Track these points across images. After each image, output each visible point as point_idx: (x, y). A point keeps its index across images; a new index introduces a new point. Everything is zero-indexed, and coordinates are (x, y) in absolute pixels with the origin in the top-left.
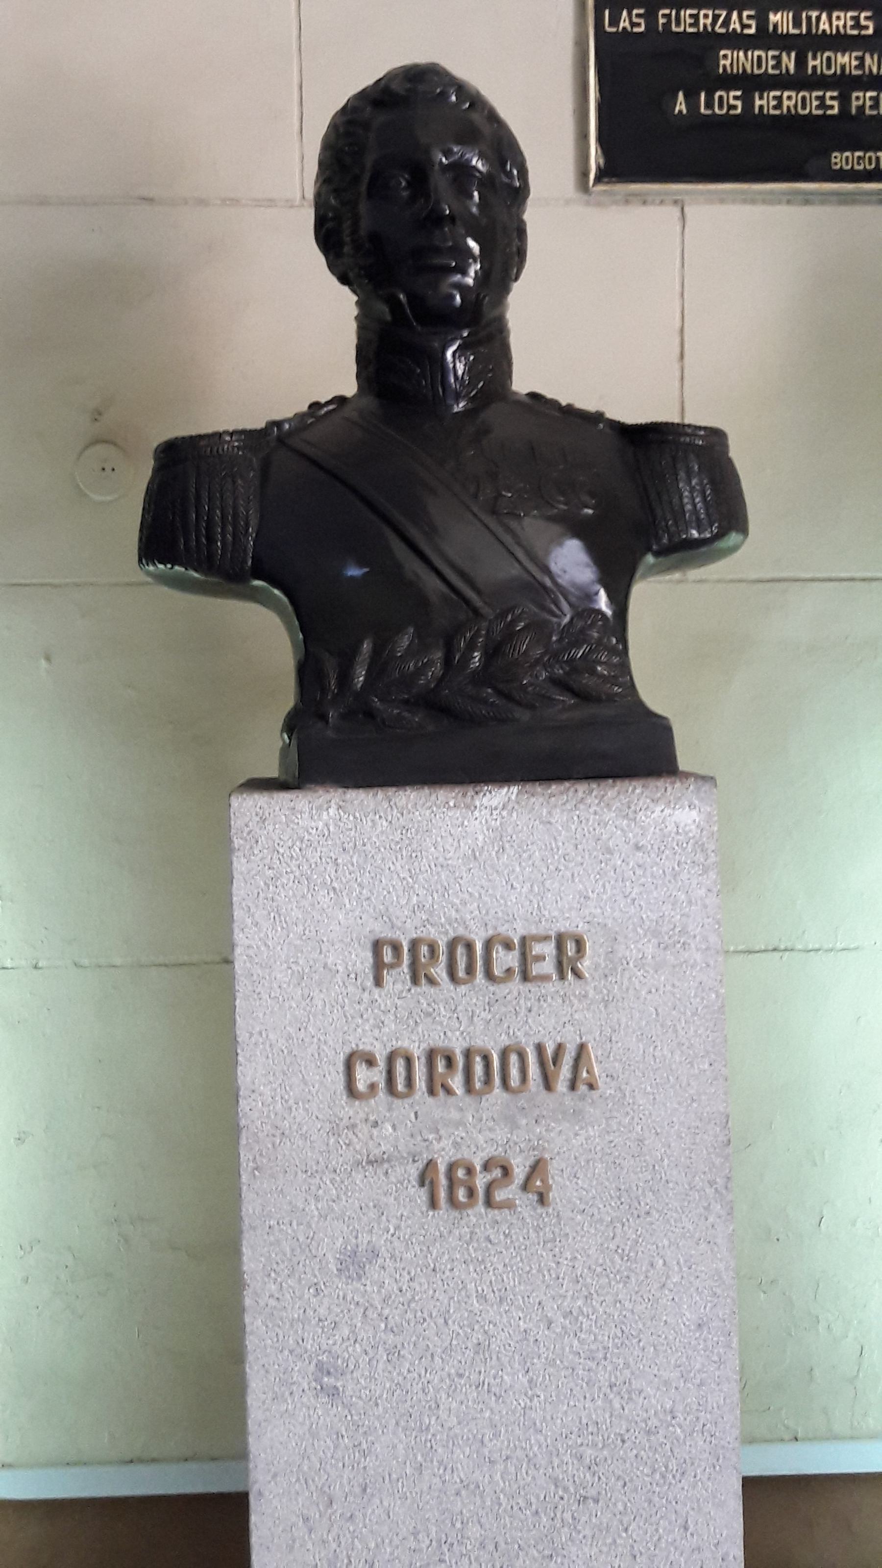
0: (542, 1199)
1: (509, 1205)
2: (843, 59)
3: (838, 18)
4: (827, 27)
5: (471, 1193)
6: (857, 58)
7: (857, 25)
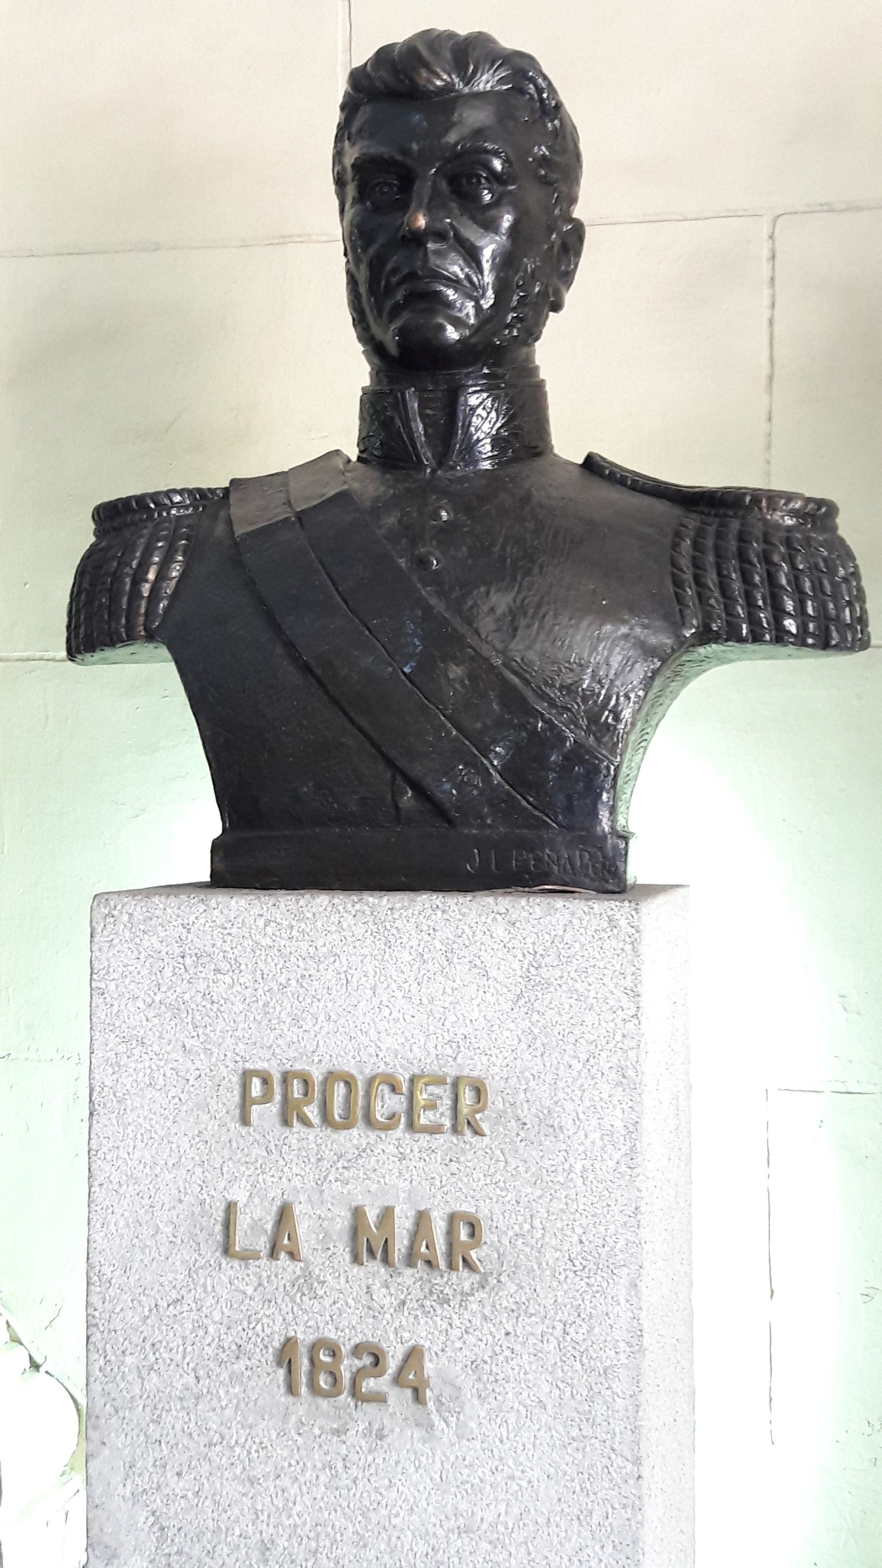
0: (418, 1396)
1: (379, 1398)
5: (335, 1378)
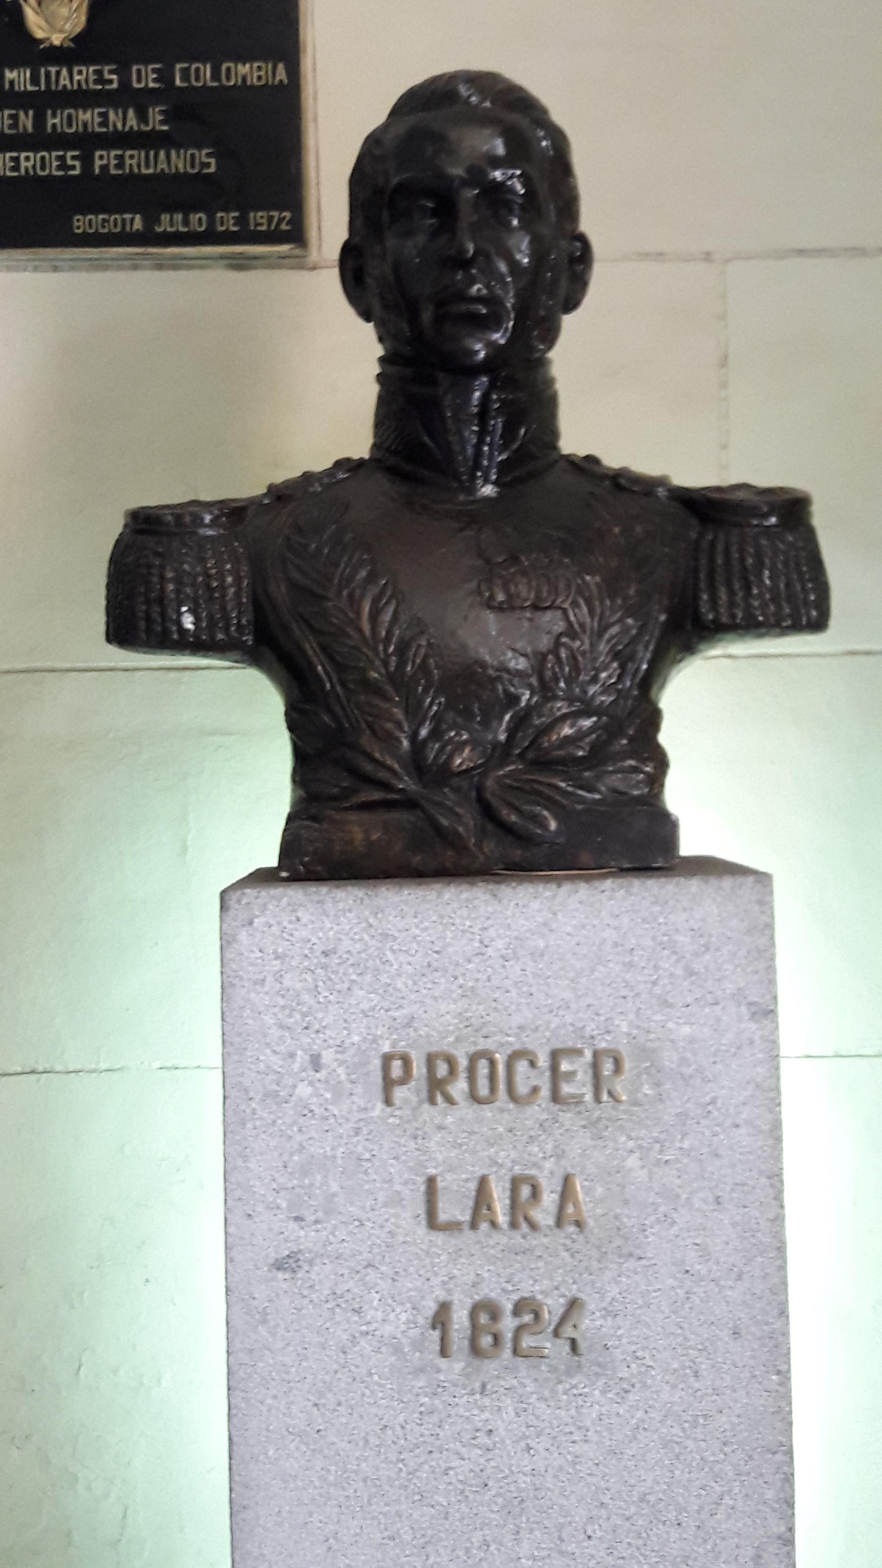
2: (85, 116)
3: (259, 68)
4: (67, 83)
5: (497, 1339)
6: (100, 114)
7: (101, 80)
